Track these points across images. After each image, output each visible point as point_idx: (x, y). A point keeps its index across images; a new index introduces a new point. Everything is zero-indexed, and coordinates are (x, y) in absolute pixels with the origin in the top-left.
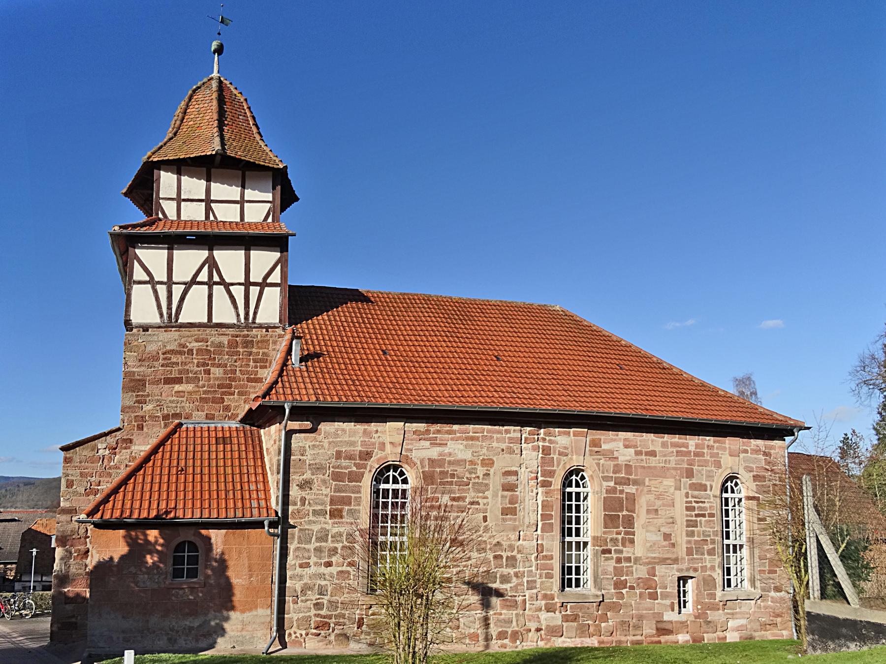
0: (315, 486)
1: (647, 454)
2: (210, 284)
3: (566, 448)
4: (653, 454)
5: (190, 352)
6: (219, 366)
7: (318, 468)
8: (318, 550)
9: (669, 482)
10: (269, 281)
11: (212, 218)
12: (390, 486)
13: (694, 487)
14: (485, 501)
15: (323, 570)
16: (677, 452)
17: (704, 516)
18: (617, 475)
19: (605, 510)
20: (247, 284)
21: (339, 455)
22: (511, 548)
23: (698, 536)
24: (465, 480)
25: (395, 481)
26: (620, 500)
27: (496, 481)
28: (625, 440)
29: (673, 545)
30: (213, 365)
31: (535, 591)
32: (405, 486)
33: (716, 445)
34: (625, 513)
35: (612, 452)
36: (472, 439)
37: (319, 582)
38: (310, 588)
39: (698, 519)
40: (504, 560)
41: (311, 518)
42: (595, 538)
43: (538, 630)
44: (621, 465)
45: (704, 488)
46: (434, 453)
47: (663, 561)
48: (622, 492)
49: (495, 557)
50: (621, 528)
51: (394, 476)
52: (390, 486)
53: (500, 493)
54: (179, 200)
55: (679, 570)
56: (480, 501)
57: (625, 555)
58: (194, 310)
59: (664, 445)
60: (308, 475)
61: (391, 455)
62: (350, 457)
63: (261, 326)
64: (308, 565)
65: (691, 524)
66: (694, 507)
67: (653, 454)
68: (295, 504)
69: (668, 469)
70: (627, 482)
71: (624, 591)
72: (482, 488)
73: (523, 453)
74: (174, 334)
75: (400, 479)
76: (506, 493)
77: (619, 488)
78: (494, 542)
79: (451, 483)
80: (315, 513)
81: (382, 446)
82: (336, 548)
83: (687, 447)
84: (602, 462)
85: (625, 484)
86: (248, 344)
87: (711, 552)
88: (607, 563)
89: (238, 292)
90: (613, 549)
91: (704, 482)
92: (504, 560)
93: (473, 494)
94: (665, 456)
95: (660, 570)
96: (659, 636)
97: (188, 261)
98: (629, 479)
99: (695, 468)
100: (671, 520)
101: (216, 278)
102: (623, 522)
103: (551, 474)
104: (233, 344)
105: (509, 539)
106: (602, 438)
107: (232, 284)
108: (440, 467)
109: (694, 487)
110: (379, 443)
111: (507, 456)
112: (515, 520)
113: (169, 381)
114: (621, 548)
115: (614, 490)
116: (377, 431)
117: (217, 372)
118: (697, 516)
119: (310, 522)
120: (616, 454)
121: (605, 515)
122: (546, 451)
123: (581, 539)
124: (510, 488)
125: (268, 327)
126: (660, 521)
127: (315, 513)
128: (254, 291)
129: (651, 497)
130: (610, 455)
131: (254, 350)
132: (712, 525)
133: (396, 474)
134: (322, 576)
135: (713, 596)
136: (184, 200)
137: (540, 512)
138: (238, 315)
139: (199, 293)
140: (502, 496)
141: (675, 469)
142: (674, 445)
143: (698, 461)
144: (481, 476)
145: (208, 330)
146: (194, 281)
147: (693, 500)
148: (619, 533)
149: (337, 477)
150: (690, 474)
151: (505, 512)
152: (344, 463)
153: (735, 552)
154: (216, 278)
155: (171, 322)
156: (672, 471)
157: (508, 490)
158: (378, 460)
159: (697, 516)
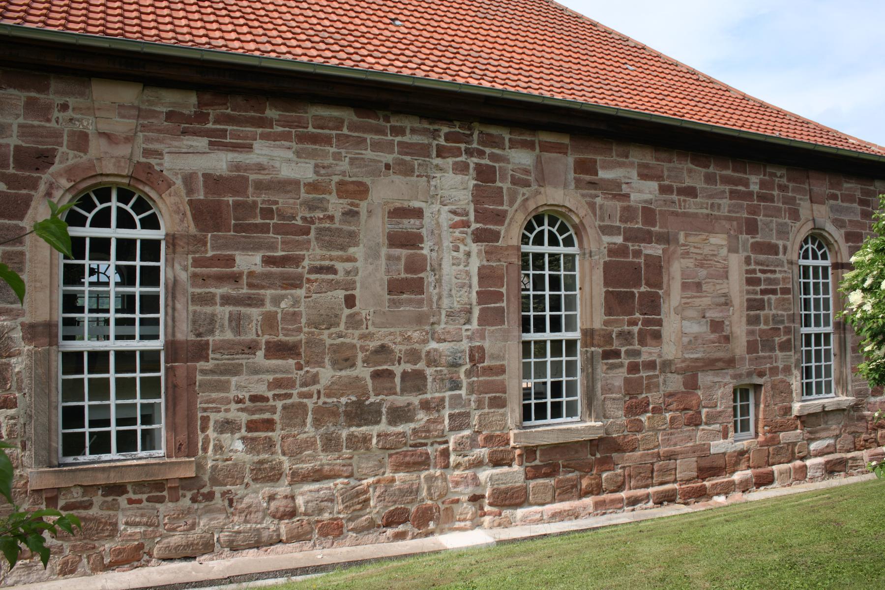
3: (527, 172)
9: (718, 240)
13: (758, 248)
14: (349, 266)
16: (732, 192)
17: (774, 292)
18: (629, 225)
19: (606, 284)
22: (413, 356)
23: (766, 323)
24: (299, 222)
26: (636, 268)
27: (374, 227)
28: (641, 166)
29: (727, 339)
31: (467, 432)
33: (791, 185)
34: (643, 289)
35: (617, 184)
36: (314, 139)
39: (766, 297)
40: (398, 380)
42: (588, 334)
43: (475, 499)
44: (635, 209)
45: (772, 249)
46: (220, 162)
47: (710, 365)
48: (637, 253)
49: (376, 375)
50: (637, 315)
51: (813, 249)
53: (384, 251)
55: (735, 377)
56: (339, 266)
57: (645, 357)
61: (111, 161)
65: (754, 305)
66: (759, 279)
67: (691, 192)
69: (717, 218)
70: (647, 237)
71: (644, 418)
72: (340, 239)
75: (560, 238)
76: (397, 251)
77: (632, 247)
78: (373, 345)
79: (264, 229)
83: (747, 185)
84: (598, 200)
85: (643, 240)
87: (785, 346)
88: (612, 373)
90: (623, 349)
91: (774, 241)
92: (398, 380)
93: (319, 252)
94: (711, 197)
95: (705, 379)
96: (703, 479)
98: (649, 233)
99: (760, 218)
100: (723, 300)
102: (641, 305)
103: (500, 217)
105: (409, 338)
106: (599, 158)
108: (236, 192)
109: (758, 248)
110: (72, 134)
111: (398, 179)
112: (420, 303)
114: (637, 347)
115: (620, 251)
116: (64, 107)
118: (764, 292)
120: (625, 189)
121: (607, 292)
122: (485, 175)
123: (564, 335)
126: (706, 301)
129: (689, 263)
130: (614, 190)
132: (787, 306)
133: (554, 230)
135: (788, 410)
137: (476, 288)
140: (389, 258)
141: (729, 219)
142: (726, 180)
143: (765, 208)
144: (338, 216)
147: (758, 268)
148: (633, 323)
150: (752, 228)
151: (396, 287)
153: (818, 343)
156: (724, 222)
157: (403, 246)
159: (764, 292)
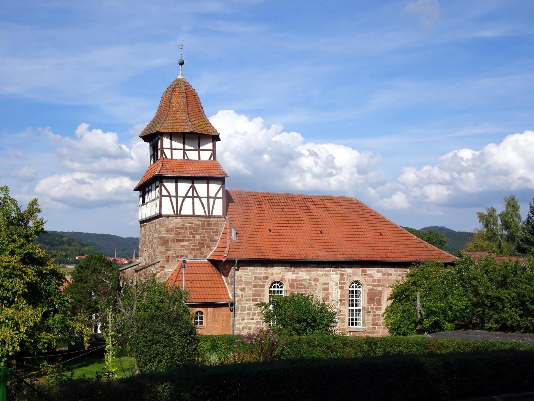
0: (246, 290)
1: (387, 275)
2: (193, 197)
4: (391, 274)
5: (186, 228)
6: (198, 234)
7: (247, 283)
8: (248, 314)
10: (217, 196)
11: (186, 158)
12: (276, 289)
15: (250, 321)
20: (208, 197)
21: (255, 278)
25: (278, 287)
26: (375, 293)
27: (320, 286)
30: (196, 234)
32: (281, 289)
35: (371, 274)
37: (249, 326)
38: (246, 328)
41: (245, 302)
46: (294, 276)
48: (376, 290)
52: (276, 289)
53: (322, 291)
54: (172, 149)
57: (377, 313)
58: (187, 210)
59: (395, 271)
60: (243, 286)
61: (276, 277)
62: (260, 279)
63: (215, 217)
64: (244, 319)
68: (239, 297)
70: (378, 286)
71: (376, 327)
73: (333, 276)
74: (179, 220)
79: (301, 288)
80: (247, 300)
81: (272, 274)
82: (255, 313)
86: (209, 224)
89: (205, 201)
97: (184, 187)
101: (195, 195)
104: (203, 225)
107: (202, 197)
113: (179, 241)
115: (372, 289)
117: (198, 237)
119: (245, 303)
120: (373, 275)
122: (342, 275)
123: (358, 308)
124: (326, 289)
125: (218, 217)
127: (247, 300)
128: (211, 201)
130: (371, 276)
131: (212, 227)
134: (249, 323)
136: (174, 149)
138: (205, 211)
139: (188, 201)
145: (194, 219)
146: (186, 196)
149: (255, 286)
152: (258, 281)
154: (195, 195)
155: (177, 214)
158: (271, 280)
